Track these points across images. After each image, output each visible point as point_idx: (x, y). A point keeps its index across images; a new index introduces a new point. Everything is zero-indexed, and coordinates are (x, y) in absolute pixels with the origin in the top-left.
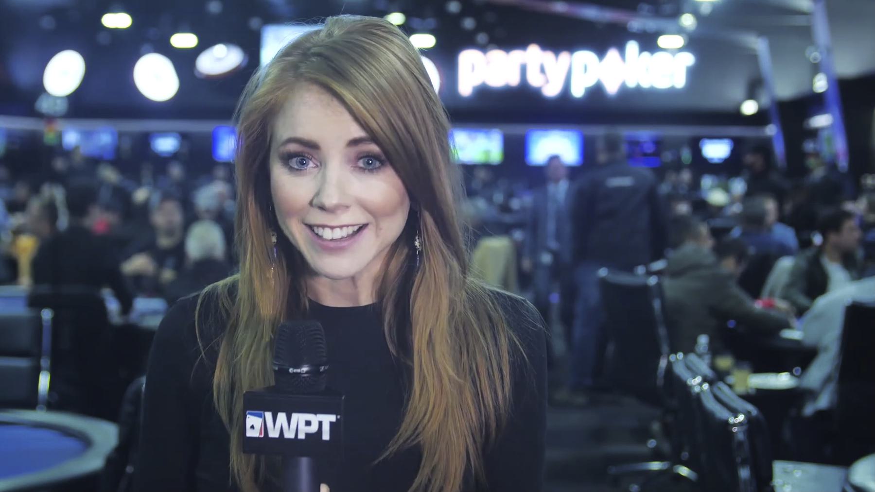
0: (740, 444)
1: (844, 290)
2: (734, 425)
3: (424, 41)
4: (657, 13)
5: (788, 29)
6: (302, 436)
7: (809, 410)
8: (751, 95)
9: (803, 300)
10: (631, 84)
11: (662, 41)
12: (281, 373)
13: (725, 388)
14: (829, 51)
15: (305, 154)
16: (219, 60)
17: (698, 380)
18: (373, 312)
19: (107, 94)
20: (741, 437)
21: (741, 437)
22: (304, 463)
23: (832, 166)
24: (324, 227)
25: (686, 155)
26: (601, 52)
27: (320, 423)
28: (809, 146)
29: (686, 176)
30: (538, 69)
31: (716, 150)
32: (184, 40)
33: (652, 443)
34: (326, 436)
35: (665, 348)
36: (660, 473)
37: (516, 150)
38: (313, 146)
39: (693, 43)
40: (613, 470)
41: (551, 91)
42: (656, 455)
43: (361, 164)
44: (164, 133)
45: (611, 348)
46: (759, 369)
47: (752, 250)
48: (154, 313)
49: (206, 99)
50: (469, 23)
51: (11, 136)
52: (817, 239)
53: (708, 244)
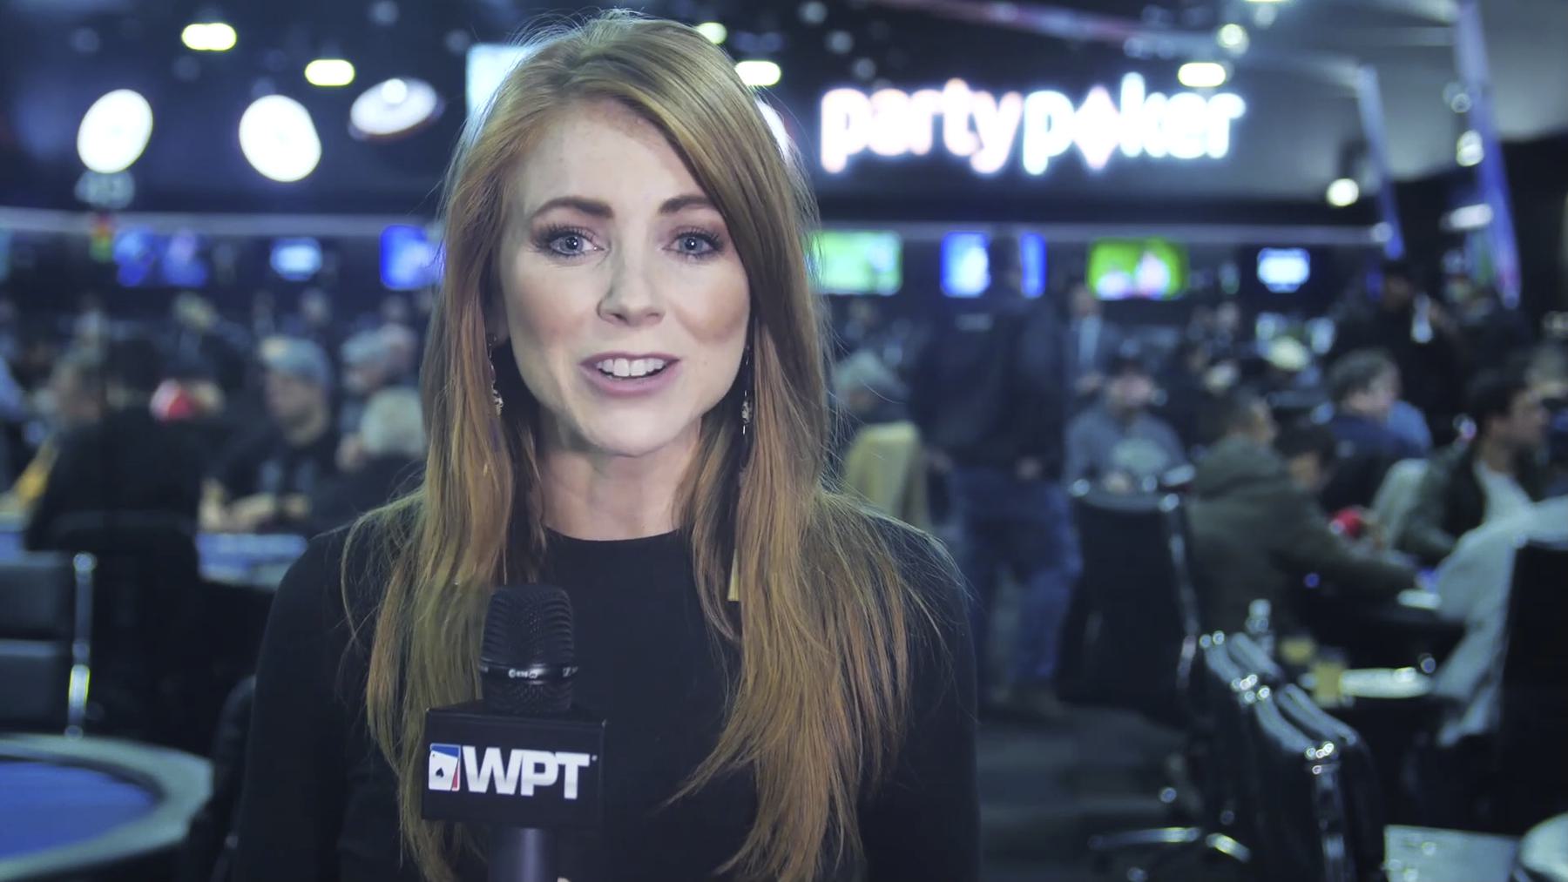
0: (1327, 796)
1: (1514, 518)
2: (1316, 762)
3: (762, 73)
4: (1178, 24)
5: (1412, 52)
6: (527, 791)
7: (1449, 734)
8: (1346, 170)
9: (1436, 538)
10: (1131, 151)
11: (1187, 73)
12: (495, 678)
13: (1299, 697)
14: (1486, 92)
15: (576, 229)
16: (393, 107)
17: (1251, 680)
18: (667, 552)
19: (192, 166)
20: (1328, 783)
21: (1328, 783)
22: (531, 837)
23: (1491, 291)
24: (615, 356)
25: (1229, 277)
26: (1077, 93)
27: (562, 769)
28: (1453, 262)
29: (1228, 316)
30: (964, 124)
31: (1284, 270)
32: (330, 72)
33: (1168, 795)
34: (571, 792)
35: (1192, 624)
36: (1183, 847)
37: (924, 268)
38: (599, 211)
39: (1243, 78)
40: (1099, 843)
41: (988, 162)
42: (1176, 817)
43: (676, 246)
44: (293, 239)
45: (1094, 626)
46: (1360, 661)
47: (1345, 449)
48: (278, 560)
49: (371, 181)
50: (840, 42)
51: (19, 243)
52: (1466, 428)
53: (1266, 433)
